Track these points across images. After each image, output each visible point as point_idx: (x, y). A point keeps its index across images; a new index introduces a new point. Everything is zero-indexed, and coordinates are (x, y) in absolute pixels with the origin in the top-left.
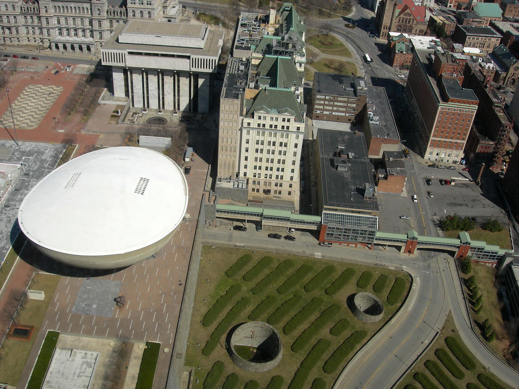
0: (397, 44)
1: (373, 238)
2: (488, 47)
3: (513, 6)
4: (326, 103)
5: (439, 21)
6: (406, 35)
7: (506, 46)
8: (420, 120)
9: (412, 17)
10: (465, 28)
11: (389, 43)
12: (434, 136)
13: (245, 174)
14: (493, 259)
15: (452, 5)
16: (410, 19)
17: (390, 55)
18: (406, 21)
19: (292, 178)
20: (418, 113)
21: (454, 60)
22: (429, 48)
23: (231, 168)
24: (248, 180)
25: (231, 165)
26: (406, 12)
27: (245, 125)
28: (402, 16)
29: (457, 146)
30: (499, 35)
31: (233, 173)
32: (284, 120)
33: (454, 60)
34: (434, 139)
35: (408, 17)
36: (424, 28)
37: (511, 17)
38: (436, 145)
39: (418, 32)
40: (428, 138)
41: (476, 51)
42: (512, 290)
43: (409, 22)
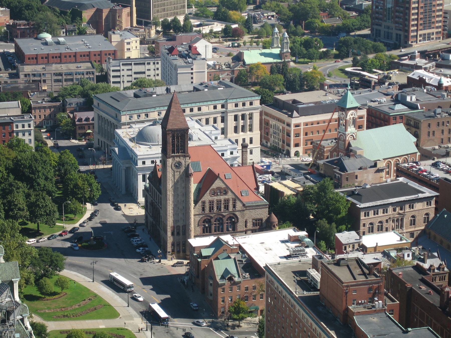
0: (215, 263)
3: (434, 123)
5: (288, 192)
6: (227, 238)
9: (230, 196)
10: (352, 194)
15: (300, 149)
16: (227, 201)
17: (204, 290)
18: (219, 208)
21: (366, 271)
22: (287, 257)
26: (214, 186)
28: (207, 197)
30: (428, 193)
33: (366, 271)
35: (222, 198)
36: (263, 214)
37: (437, 147)
39: (250, 225)
41: (390, 238)
43: (227, 207)
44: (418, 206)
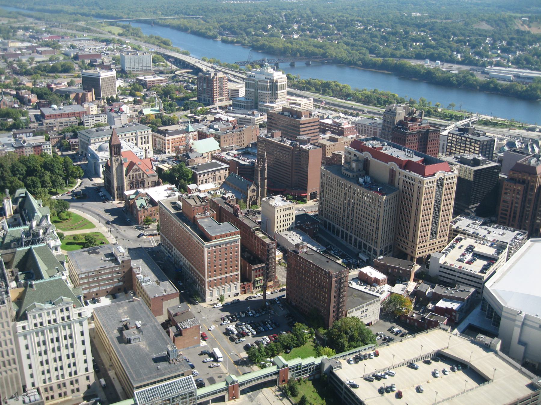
1: (195, 399)
2: (220, 179)
3: (226, 136)
4: (91, 280)
5: (166, 169)
6: (141, 190)
7: (236, 173)
8: (188, 266)
9: (141, 172)
11: (127, 202)
12: (210, 277)
13: (33, 384)
14: (306, 373)
15: (170, 150)
16: (140, 174)
18: (136, 177)
19: (87, 370)
20: (184, 261)
23: (15, 383)
24: (38, 389)
25: (14, 379)
26: (134, 168)
27: (20, 330)
28: (131, 173)
29: (232, 280)
30: (225, 166)
31: (19, 388)
32: (62, 311)
34: (210, 279)
35: (138, 173)
36: (156, 179)
38: (215, 284)
39: (150, 184)
40: (203, 281)
41: (210, 186)
42: (343, 392)
43: (140, 177)
44: (221, 172)
